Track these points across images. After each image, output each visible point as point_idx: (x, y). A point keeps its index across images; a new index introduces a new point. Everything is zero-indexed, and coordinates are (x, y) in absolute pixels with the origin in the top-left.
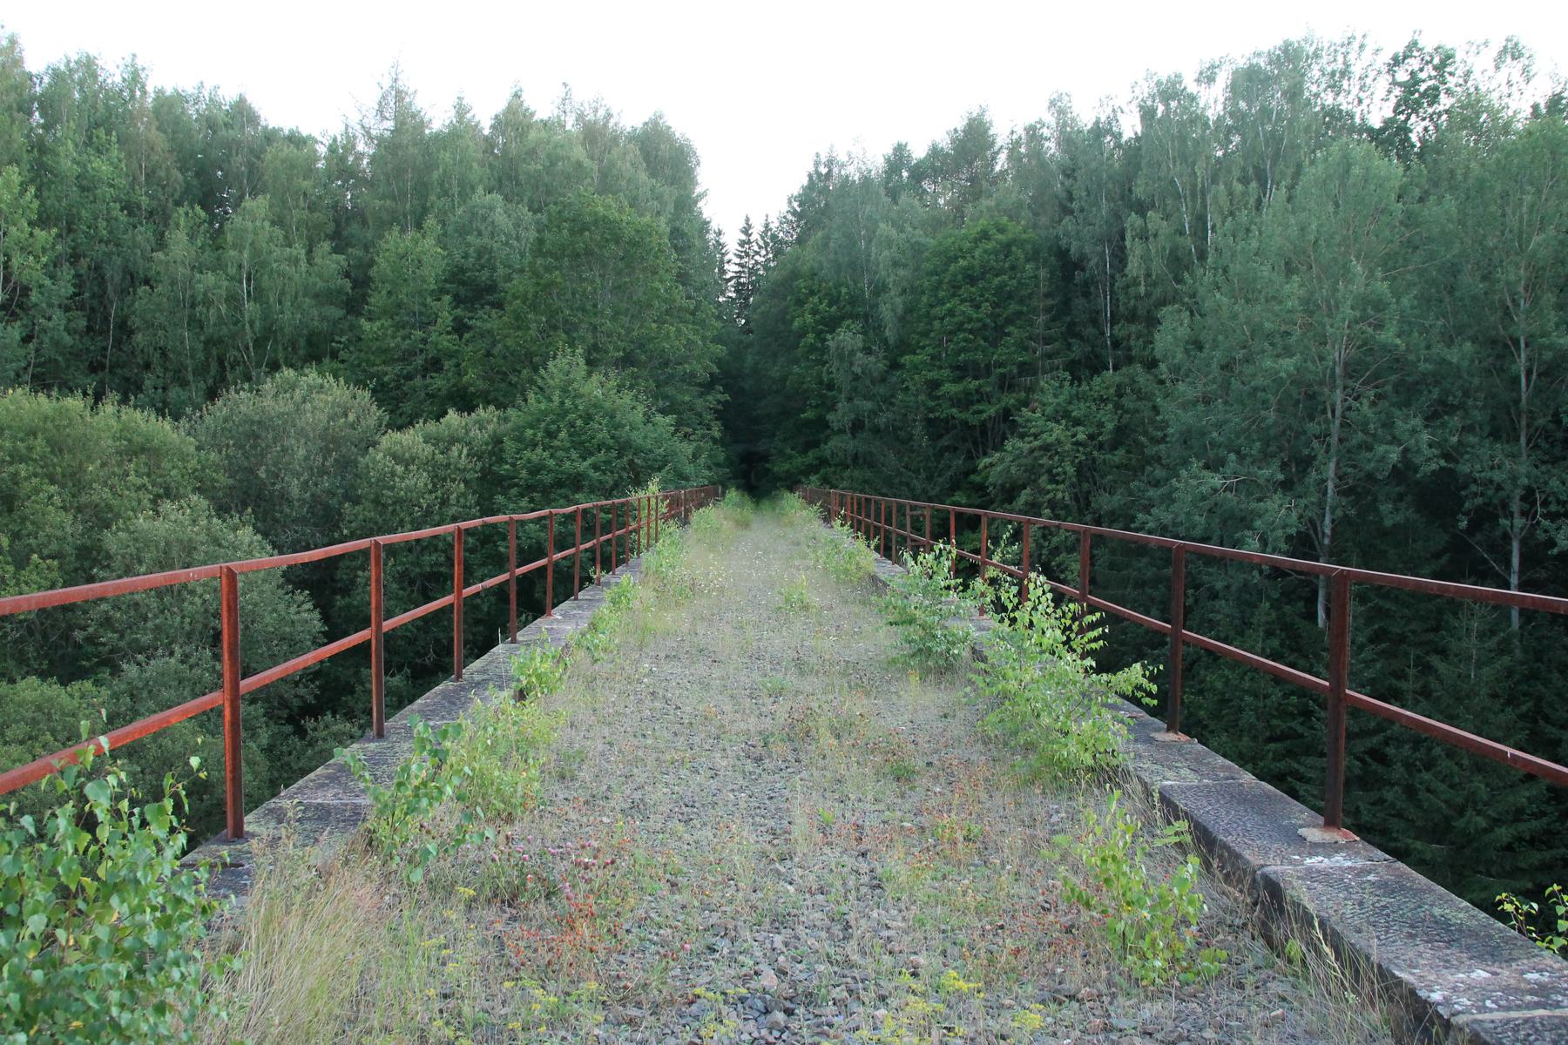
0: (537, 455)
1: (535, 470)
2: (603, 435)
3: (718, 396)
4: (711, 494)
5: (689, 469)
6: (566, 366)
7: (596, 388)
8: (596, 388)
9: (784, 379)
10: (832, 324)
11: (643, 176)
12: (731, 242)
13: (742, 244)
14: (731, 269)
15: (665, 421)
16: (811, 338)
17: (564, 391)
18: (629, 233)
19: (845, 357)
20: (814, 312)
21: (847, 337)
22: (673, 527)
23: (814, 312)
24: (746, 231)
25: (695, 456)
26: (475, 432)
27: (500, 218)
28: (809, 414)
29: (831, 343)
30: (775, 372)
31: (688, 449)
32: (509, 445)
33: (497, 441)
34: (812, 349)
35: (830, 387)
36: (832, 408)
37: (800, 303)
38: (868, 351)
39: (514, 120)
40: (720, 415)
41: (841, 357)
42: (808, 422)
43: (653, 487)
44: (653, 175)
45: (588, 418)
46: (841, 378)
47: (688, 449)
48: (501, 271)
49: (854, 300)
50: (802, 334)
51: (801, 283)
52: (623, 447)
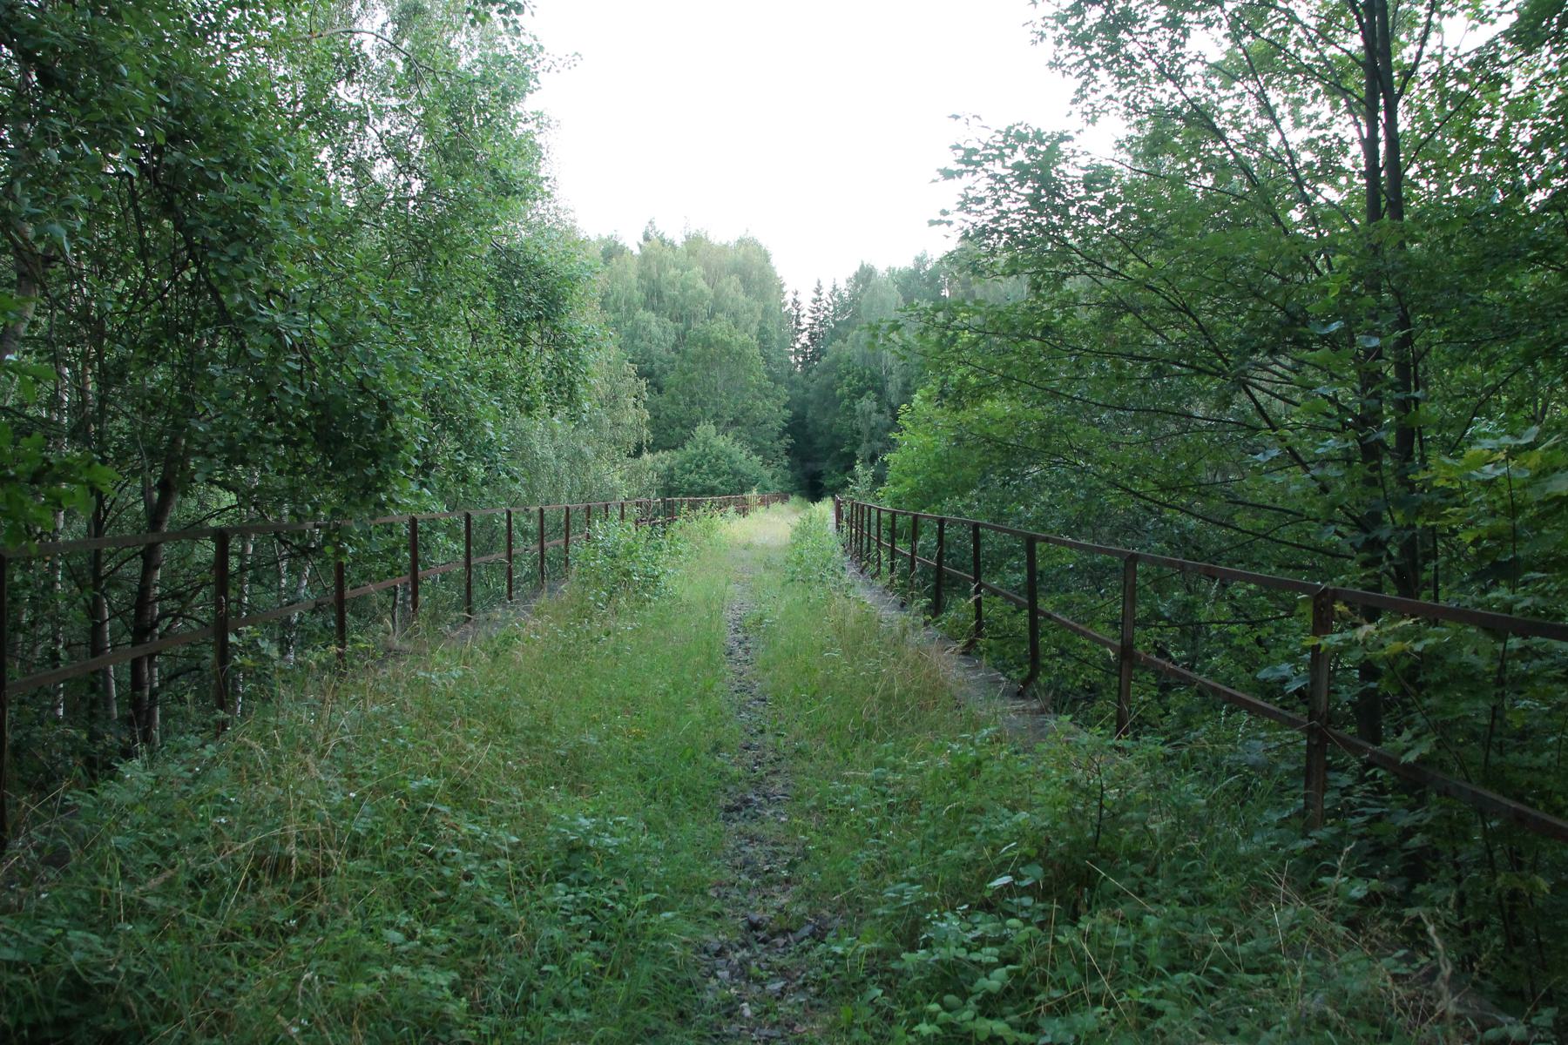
0: (694, 477)
1: (691, 485)
2: (725, 467)
3: (788, 440)
4: (784, 497)
5: (769, 484)
6: (705, 430)
7: (721, 442)
8: (721, 442)
9: (831, 426)
10: (860, 393)
11: (742, 297)
12: (806, 304)
13: (815, 301)
14: (806, 322)
15: (757, 459)
16: (846, 402)
17: (705, 443)
18: (736, 347)
19: (866, 416)
20: (849, 385)
21: (867, 403)
22: (762, 508)
23: (849, 385)
24: (818, 291)
25: (773, 477)
26: (659, 465)
27: (655, 330)
28: (845, 449)
29: (857, 407)
30: (826, 422)
31: (769, 473)
32: (678, 472)
33: (671, 469)
34: (848, 408)
35: (859, 433)
36: (858, 446)
37: (841, 378)
38: (880, 411)
39: (655, 246)
40: (788, 452)
41: (863, 415)
42: (845, 454)
43: (755, 492)
44: (747, 293)
45: (718, 458)
46: (864, 427)
47: (769, 473)
48: (657, 364)
49: (873, 378)
50: (842, 398)
51: (841, 366)
52: (736, 473)
